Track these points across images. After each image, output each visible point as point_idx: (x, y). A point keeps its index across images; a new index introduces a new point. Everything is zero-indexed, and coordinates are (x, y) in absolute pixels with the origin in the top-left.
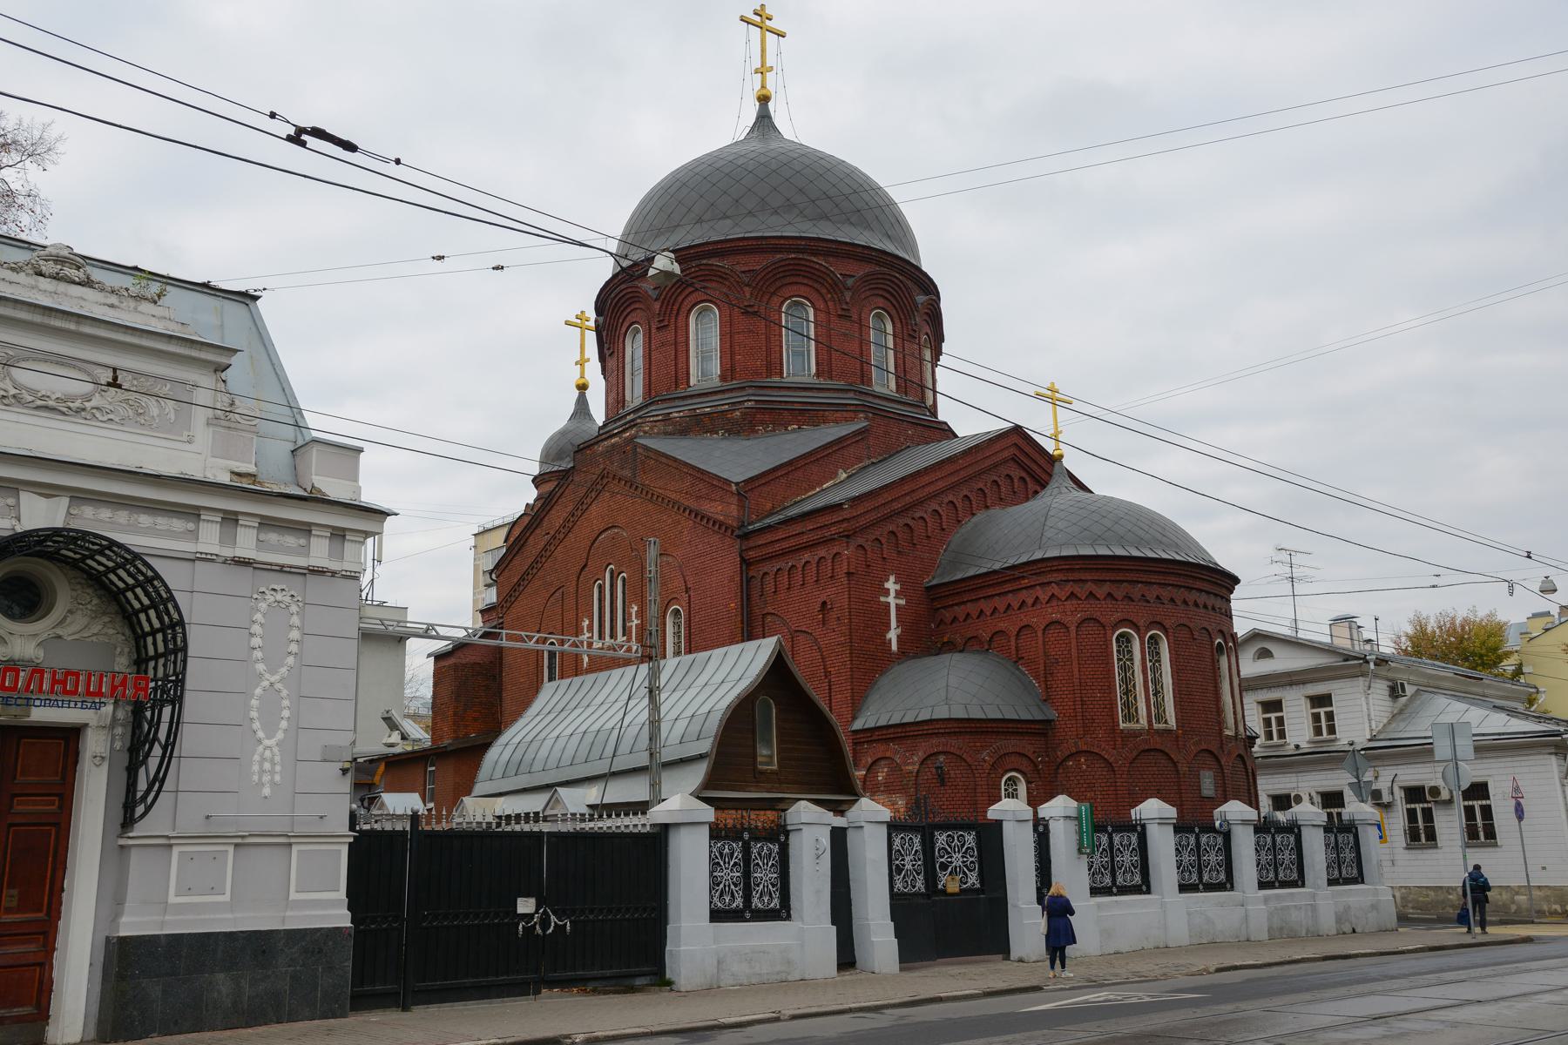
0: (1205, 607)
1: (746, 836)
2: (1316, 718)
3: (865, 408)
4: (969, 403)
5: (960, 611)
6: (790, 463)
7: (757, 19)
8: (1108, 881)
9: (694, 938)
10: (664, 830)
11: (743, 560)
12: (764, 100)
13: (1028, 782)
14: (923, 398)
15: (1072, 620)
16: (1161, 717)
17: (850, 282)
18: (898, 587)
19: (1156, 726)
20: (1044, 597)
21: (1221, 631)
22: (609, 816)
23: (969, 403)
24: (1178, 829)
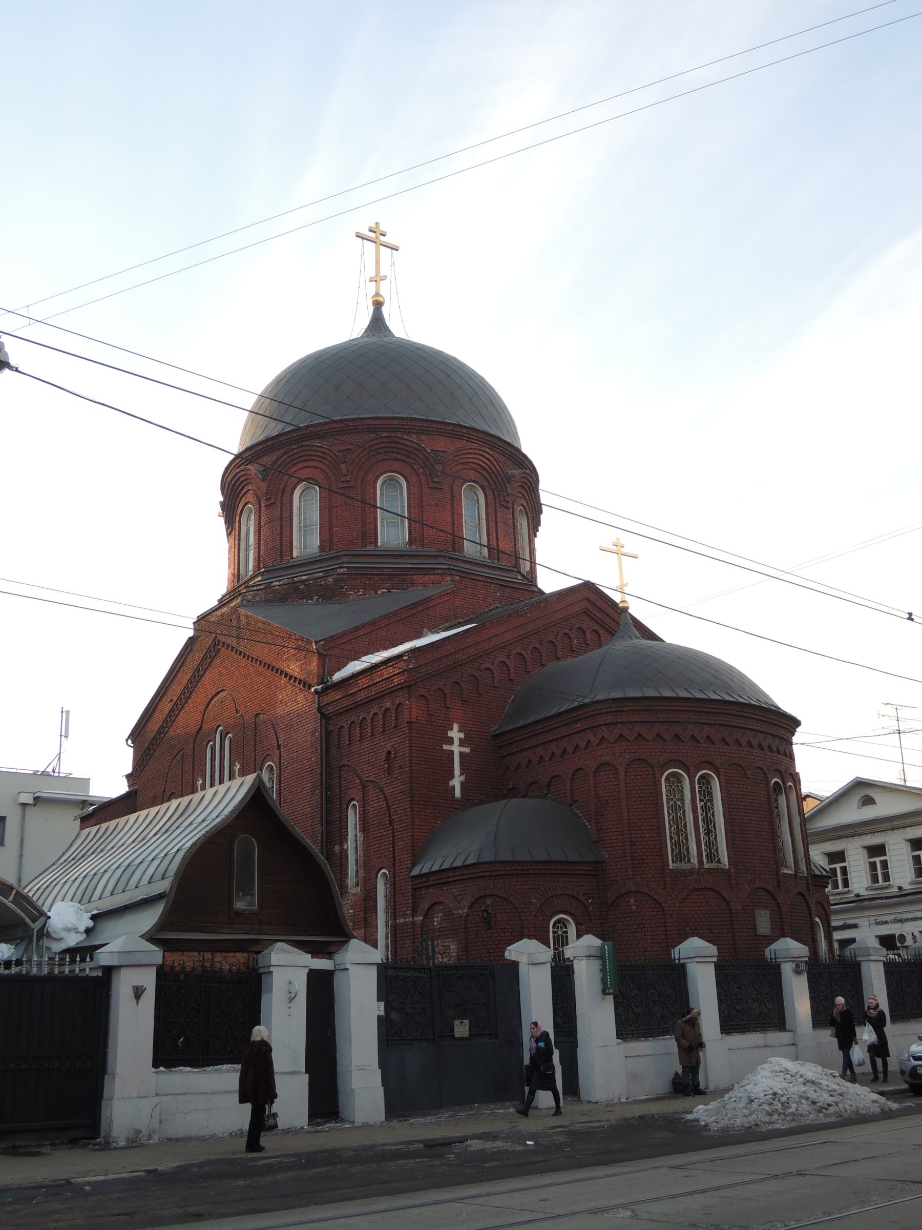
0: (760, 747)
2: (873, 866)
3: (449, 571)
4: (560, 559)
6: (373, 623)
7: (373, 235)
10: (109, 971)
11: (323, 715)
12: (378, 305)
18: (462, 735)
19: (706, 866)
22: (83, 960)
23: (560, 559)
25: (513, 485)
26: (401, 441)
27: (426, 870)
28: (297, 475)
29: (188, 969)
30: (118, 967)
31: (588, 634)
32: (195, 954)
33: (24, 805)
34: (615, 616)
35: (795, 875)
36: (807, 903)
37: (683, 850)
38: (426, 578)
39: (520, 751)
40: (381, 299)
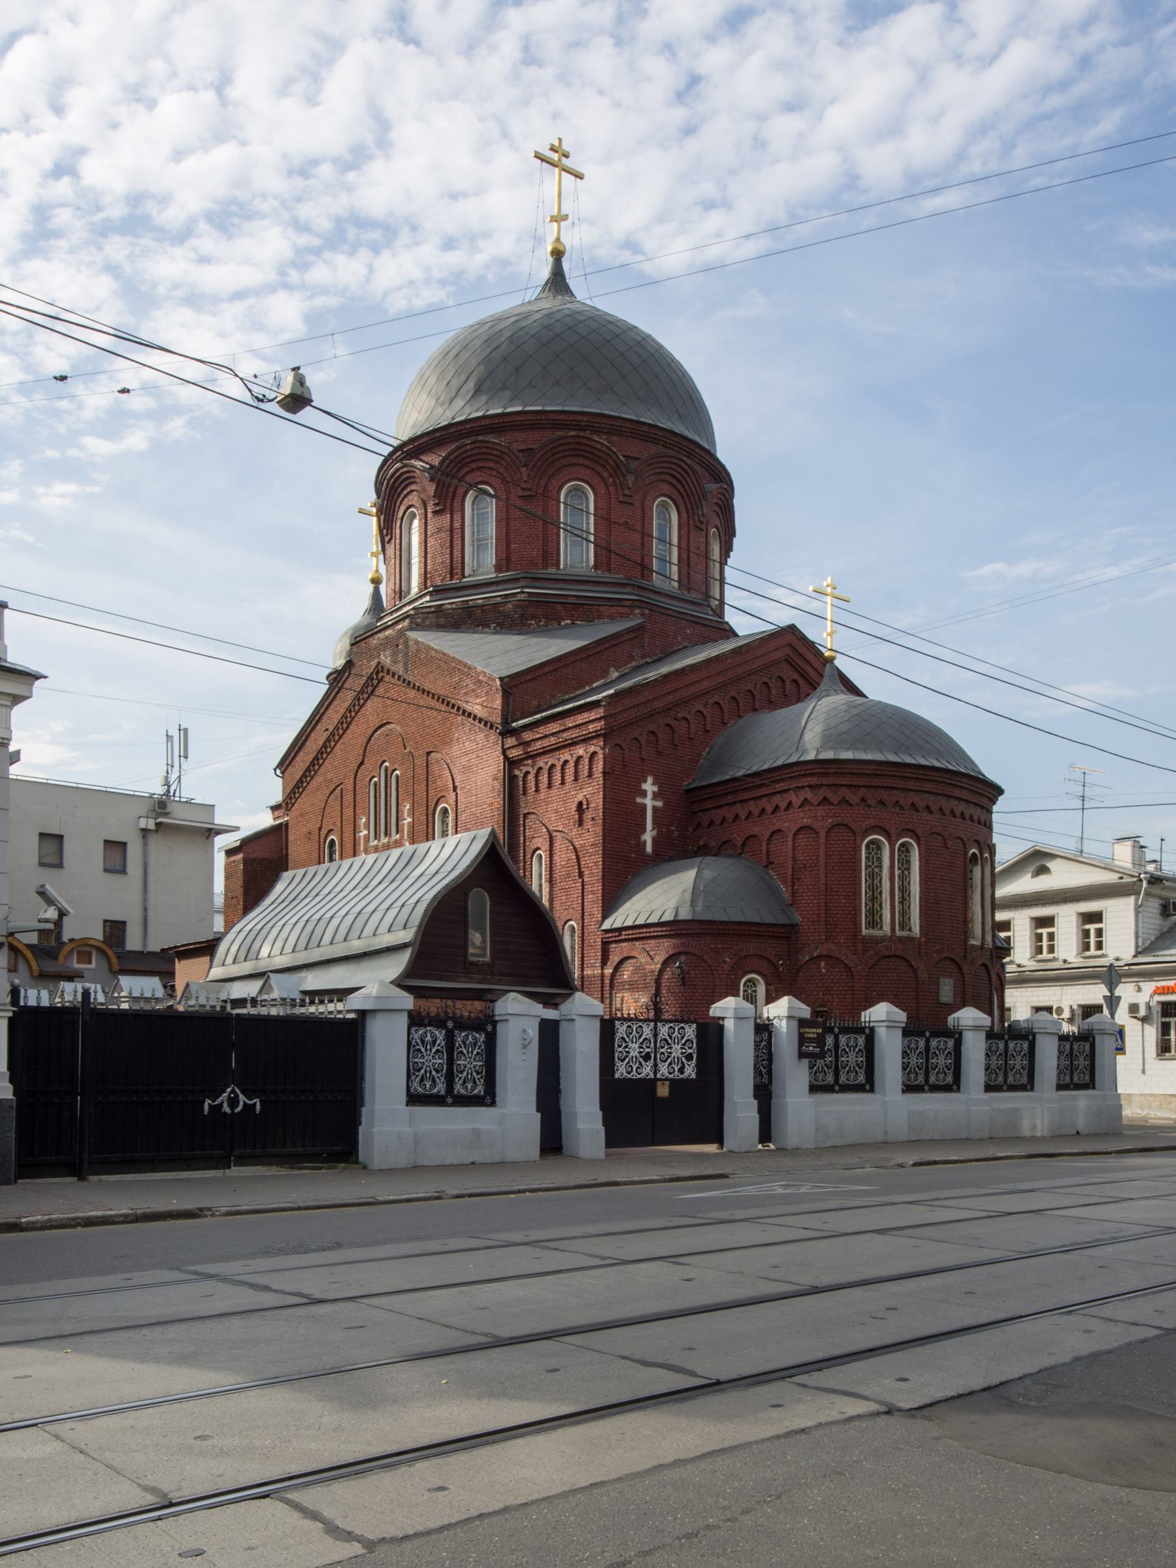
0: (963, 816)
1: (450, 1024)
3: (640, 604)
4: (754, 601)
5: (717, 815)
7: (555, 157)
8: (830, 1079)
9: (389, 1116)
10: (363, 1014)
11: (506, 757)
12: (558, 254)
13: (767, 984)
14: (707, 596)
15: (822, 826)
16: (905, 925)
17: (633, 465)
18: (655, 789)
19: (898, 933)
20: (797, 802)
21: (977, 842)
23: (754, 601)
24: (906, 1033)
25: (702, 489)
26: (589, 443)
27: (618, 925)
28: (468, 479)
29: (432, 1014)
30: (374, 1011)
31: (788, 683)
32: (438, 1001)
33: (145, 831)
34: (816, 664)
35: (982, 947)
36: (989, 973)
37: (877, 917)
38: (613, 610)
39: (714, 808)
40: (561, 249)
